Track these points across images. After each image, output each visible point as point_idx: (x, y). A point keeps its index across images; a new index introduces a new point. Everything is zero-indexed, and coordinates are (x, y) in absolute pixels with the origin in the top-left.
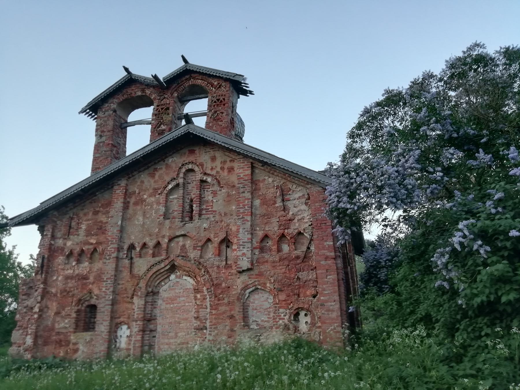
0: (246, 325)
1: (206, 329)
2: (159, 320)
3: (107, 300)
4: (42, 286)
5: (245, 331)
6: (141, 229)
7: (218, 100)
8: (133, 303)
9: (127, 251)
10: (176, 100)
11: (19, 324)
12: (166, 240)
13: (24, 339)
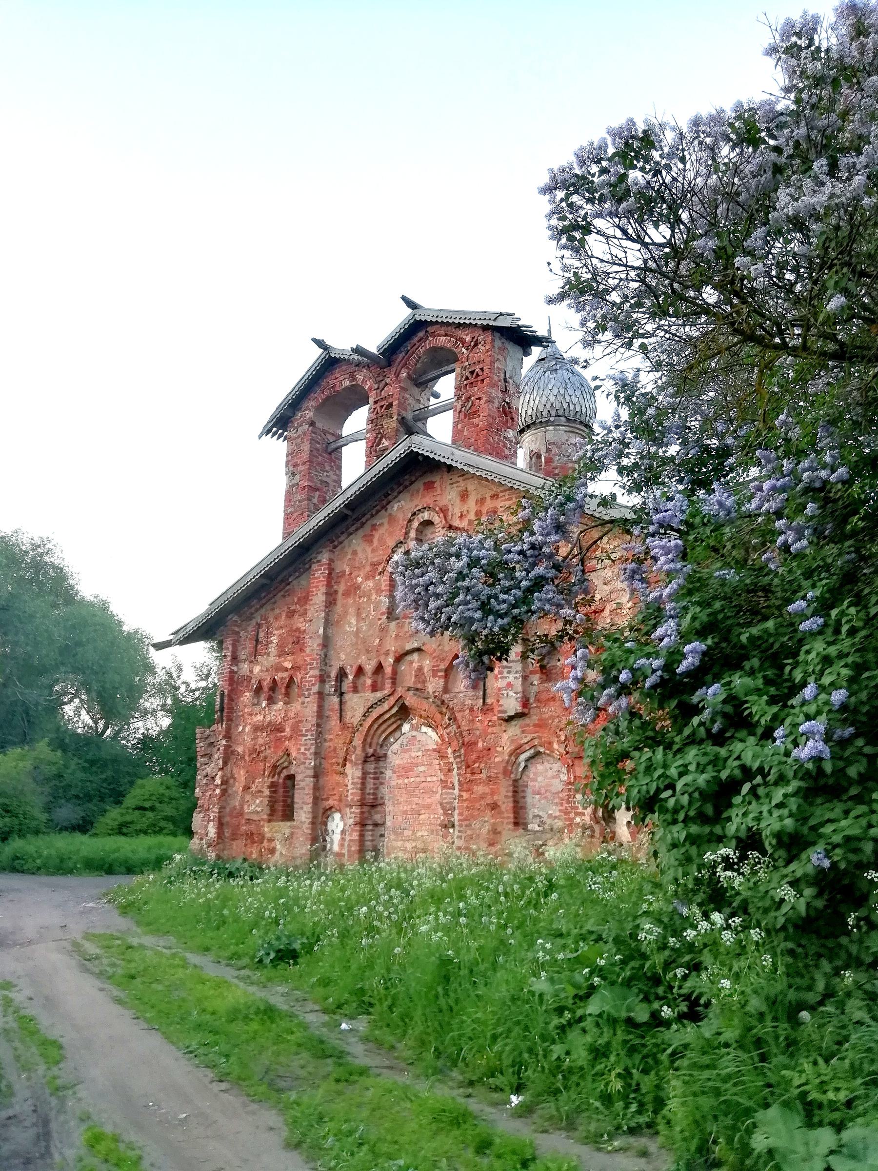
0: (519, 822)
1: (453, 826)
2: (389, 807)
3: (307, 768)
4: (224, 742)
5: (517, 833)
6: (354, 640)
7: (472, 373)
8: (343, 774)
9: (336, 681)
10: (409, 384)
11: (200, 803)
12: (391, 660)
13: (206, 827)
